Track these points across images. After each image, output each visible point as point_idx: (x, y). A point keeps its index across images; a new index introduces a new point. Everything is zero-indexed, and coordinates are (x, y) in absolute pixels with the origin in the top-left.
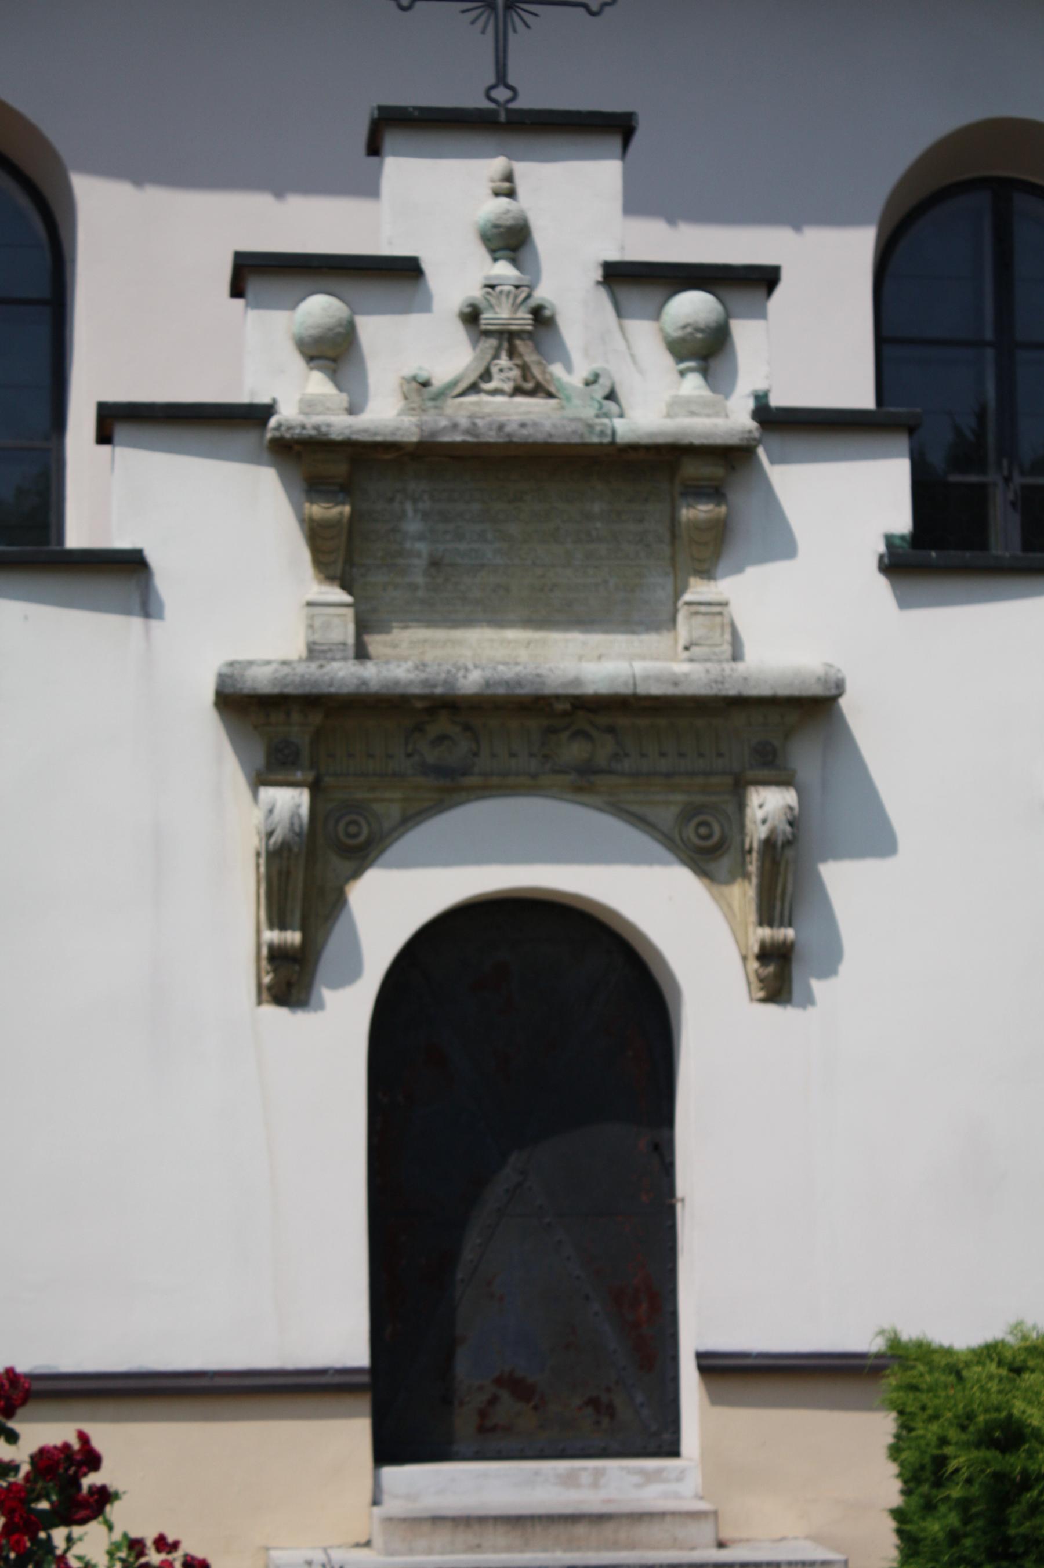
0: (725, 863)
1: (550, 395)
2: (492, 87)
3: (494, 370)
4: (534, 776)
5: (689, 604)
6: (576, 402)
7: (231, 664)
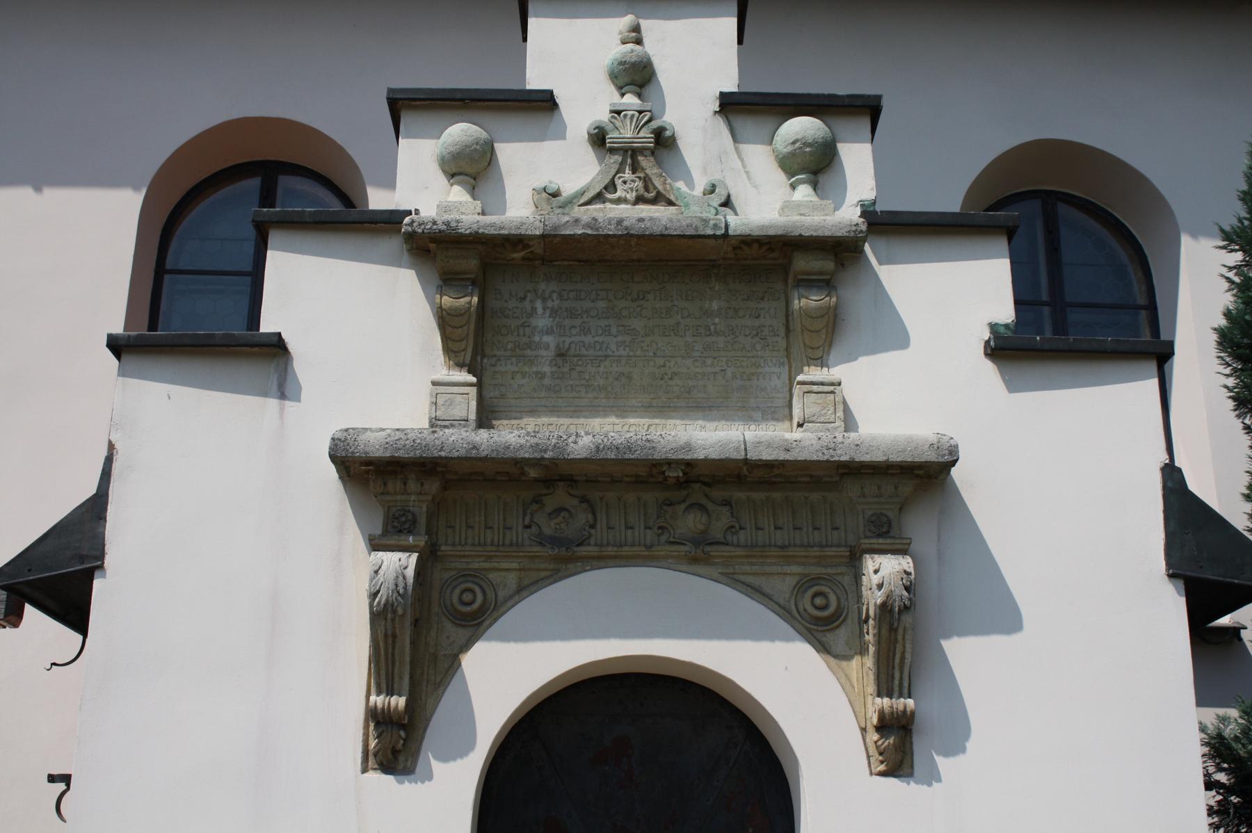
0: (840, 637)
1: (671, 203)
3: (618, 182)
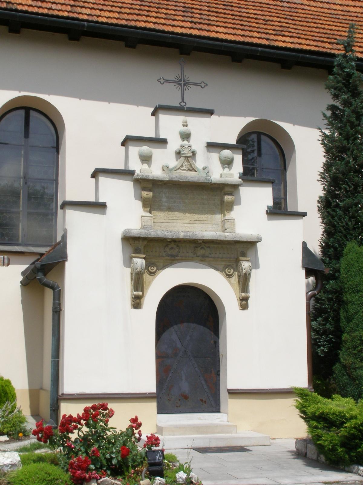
1: (196, 171)
2: (181, 102)
3: (184, 165)
4: (192, 258)
6: (202, 173)
7: (128, 229)
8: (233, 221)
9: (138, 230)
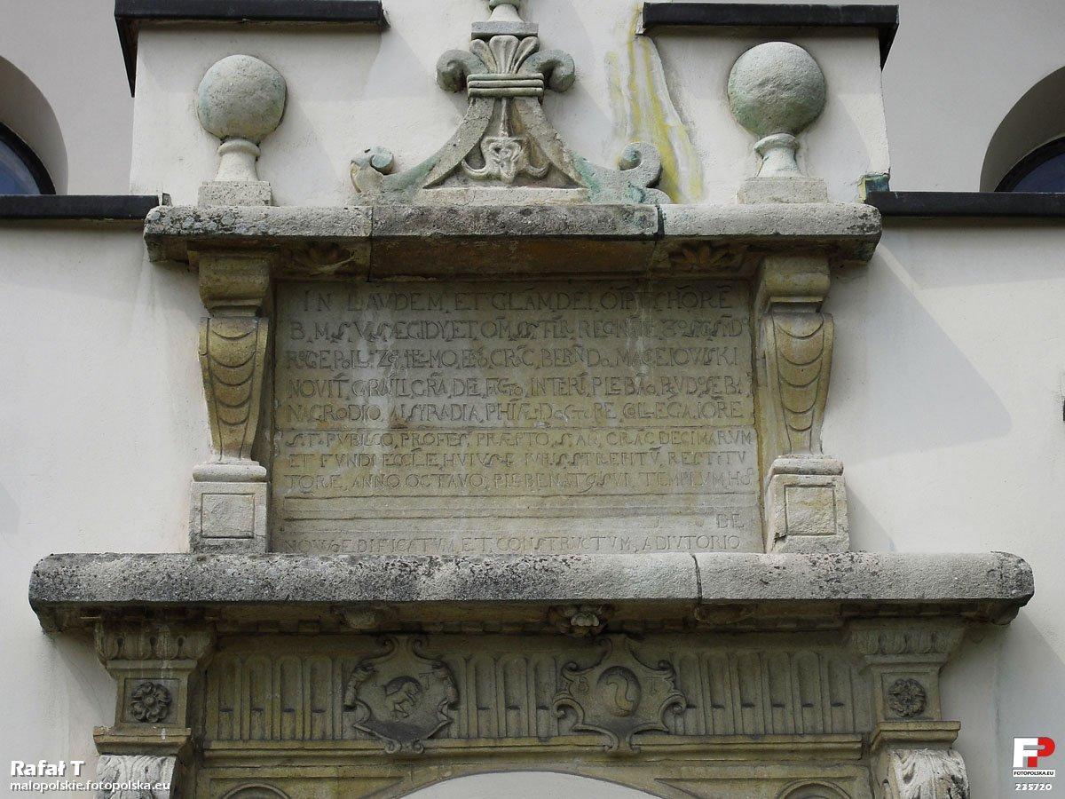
3: (487, 150)
5: (776, 471)
8: (828, 479)
9: (127, 559)
